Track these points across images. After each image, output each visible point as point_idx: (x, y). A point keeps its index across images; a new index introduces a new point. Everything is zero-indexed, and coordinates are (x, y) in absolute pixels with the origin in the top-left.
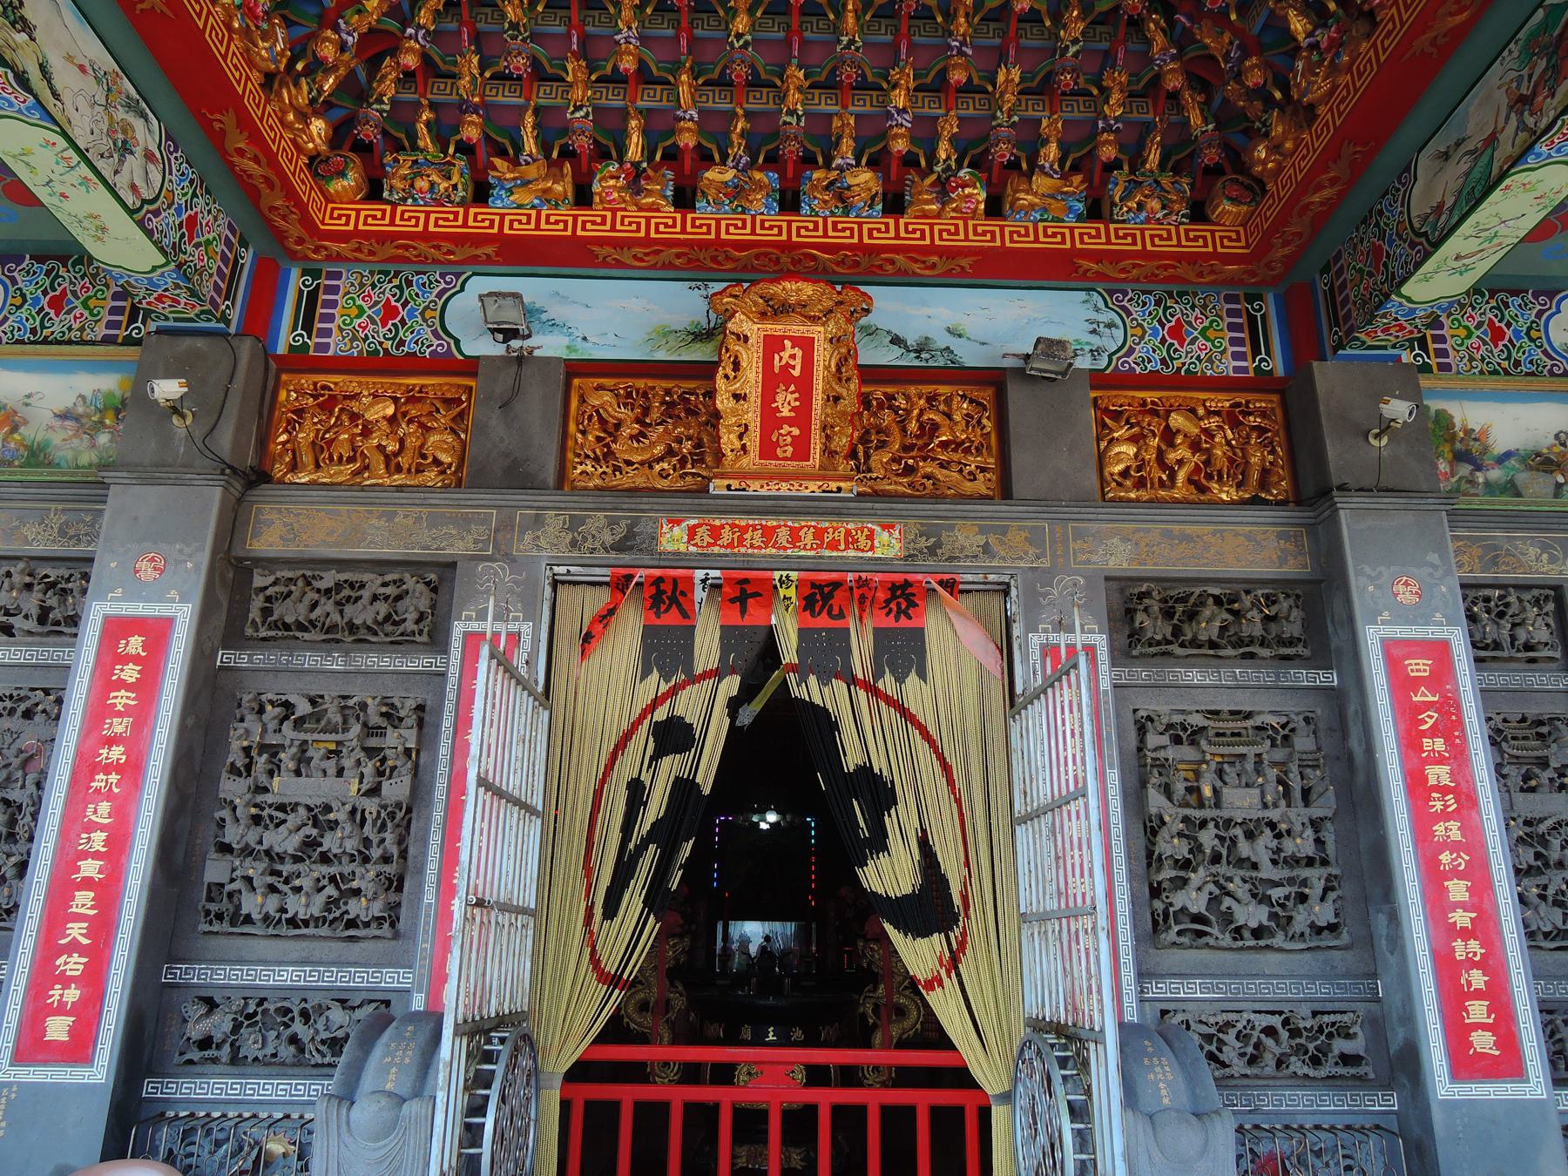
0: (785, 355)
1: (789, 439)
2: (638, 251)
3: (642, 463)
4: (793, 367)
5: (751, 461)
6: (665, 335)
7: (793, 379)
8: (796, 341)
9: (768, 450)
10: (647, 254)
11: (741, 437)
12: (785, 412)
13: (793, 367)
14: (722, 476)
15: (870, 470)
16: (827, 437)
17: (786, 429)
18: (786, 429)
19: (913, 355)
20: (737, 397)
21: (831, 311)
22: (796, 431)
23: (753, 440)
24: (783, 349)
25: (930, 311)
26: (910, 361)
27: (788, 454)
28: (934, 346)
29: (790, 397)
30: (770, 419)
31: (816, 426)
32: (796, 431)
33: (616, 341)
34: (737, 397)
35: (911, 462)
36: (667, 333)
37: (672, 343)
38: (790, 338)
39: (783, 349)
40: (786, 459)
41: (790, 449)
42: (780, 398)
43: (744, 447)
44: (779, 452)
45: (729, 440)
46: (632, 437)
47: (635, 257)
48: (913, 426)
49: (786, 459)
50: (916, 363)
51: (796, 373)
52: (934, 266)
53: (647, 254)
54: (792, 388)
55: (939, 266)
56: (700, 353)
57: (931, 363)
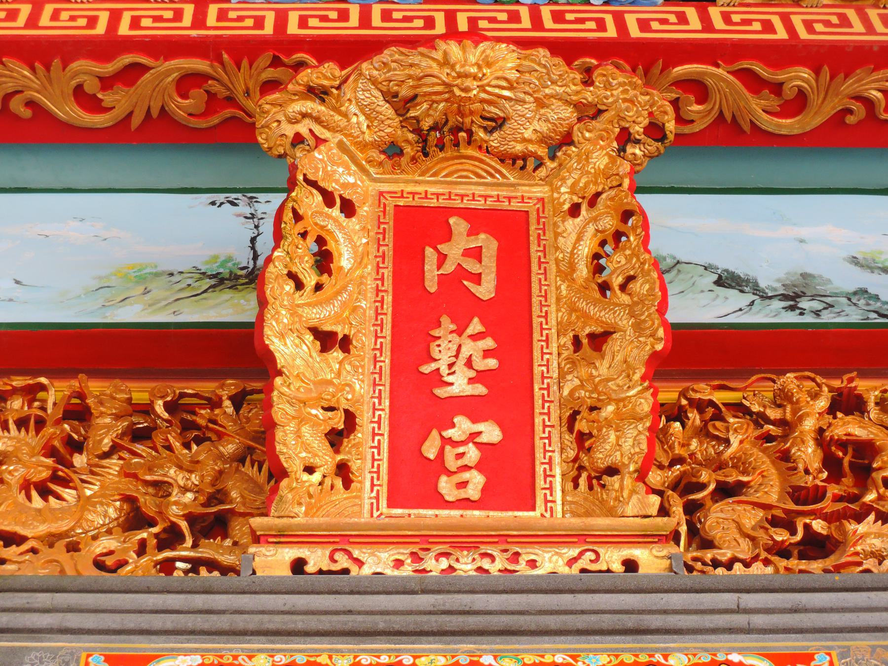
0: (454, 250)
1: (472, 454)
2: (85, 70)
3: (51, 540)
4: (477, 279)
5: (368, 500)
6: (141, 280)
7: (478, 307)
8: (479, 220)
9: (414, 480)
10: (107, 83)
11: (335, 438)
12: (460, 384)
13: (477, 279)
14: (282, 537)
15: (708, 544)
16: (581, 438)
17: (462, 426)
18: (462, 426)
19: (777, 304)
20: (326, 340)
21: (567, 140)
22: (491, 433)
23: (370, 452)
24: (448, 236)
25: (804, 232)
26: (773, 314)
27: (473, 492)
28: (829, 289)
29: (469, 348)
30: (417, 402)
31: (547, 423)
32: (491, 433)
33: (19, 292)
34: (326, 340)
35: (818, 526)
36: (145, 279)
37: (156, 293)
38: (466, 214)
39: (448, 236)
40: (466, 503)
41: (477, 480)
42: (443, 354)
43: (343, 470)
44: (445, 486)
45: (299, 442)
46: (26, 486)
47: (79, 94)
48: (808, 453)
49: (466, 503)
50: (792, 318)
51: (486, 290)
52: (798, 104)
53: (107, 83)
54: (476, 326)
55: (814, 100)
56: (229, 309)
57: (827, 317)
